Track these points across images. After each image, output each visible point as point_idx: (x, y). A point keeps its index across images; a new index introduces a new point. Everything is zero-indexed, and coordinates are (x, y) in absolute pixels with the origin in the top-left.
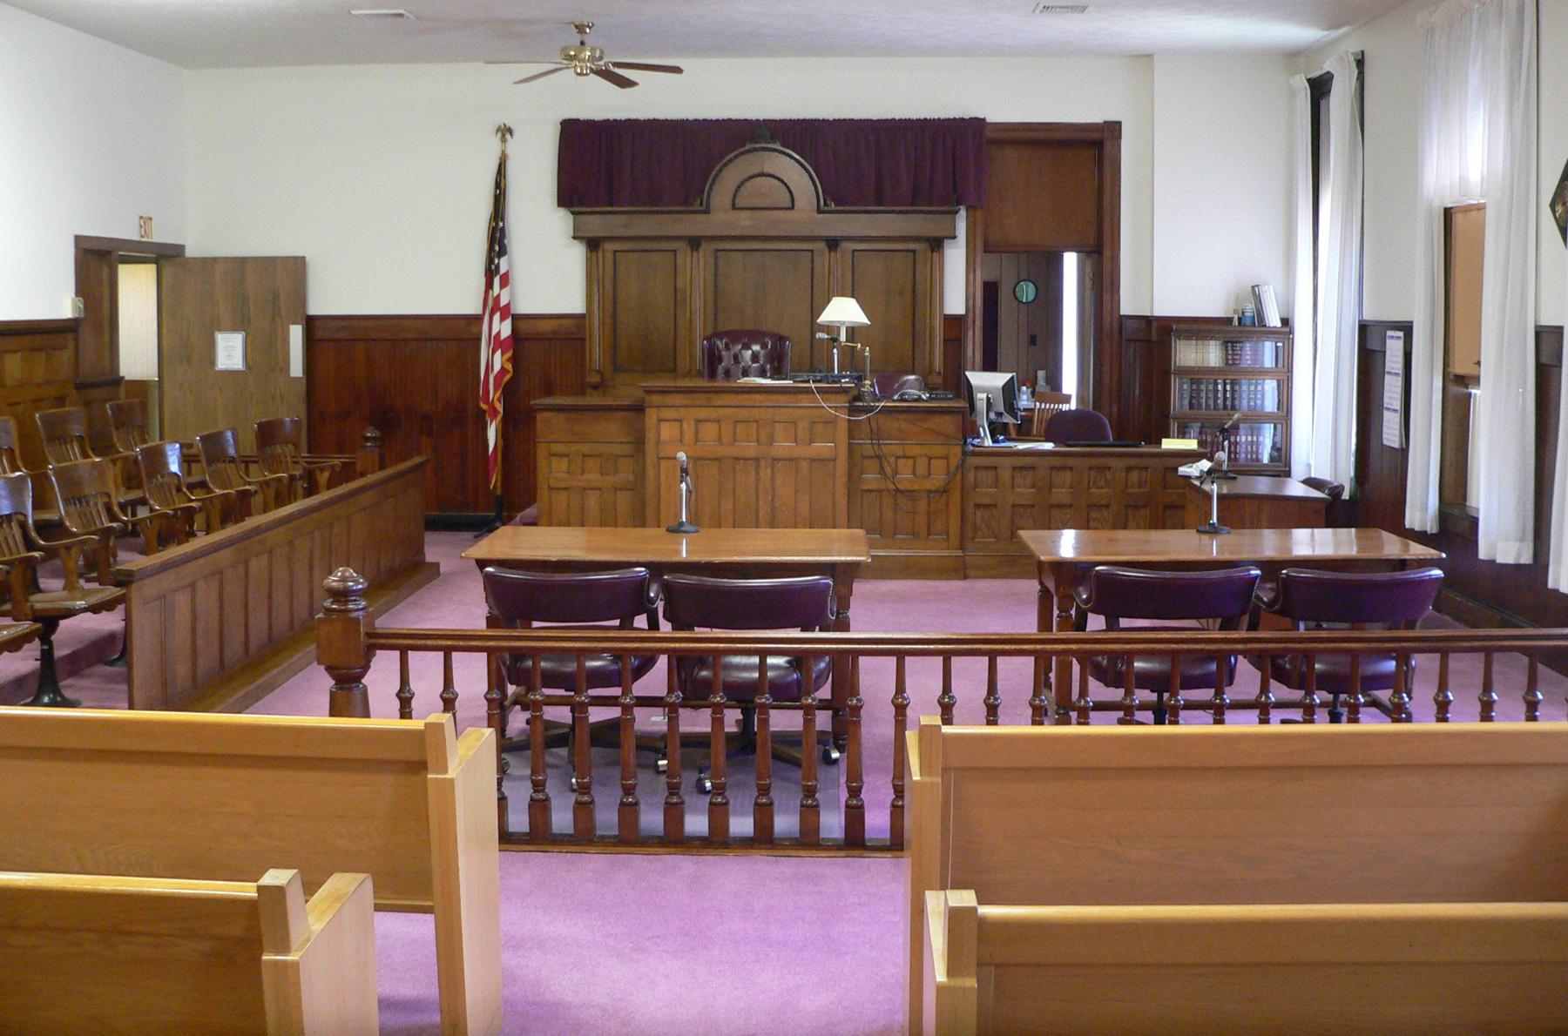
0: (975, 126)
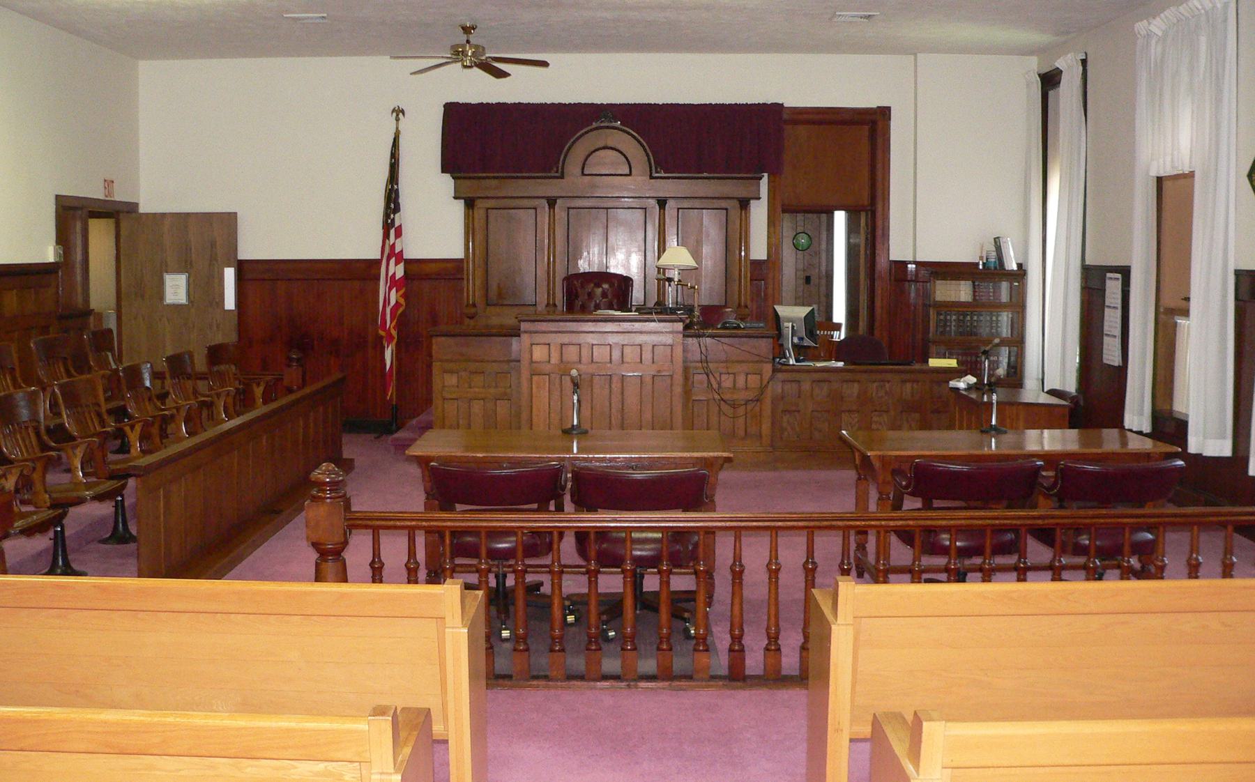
0: (775, 110)
